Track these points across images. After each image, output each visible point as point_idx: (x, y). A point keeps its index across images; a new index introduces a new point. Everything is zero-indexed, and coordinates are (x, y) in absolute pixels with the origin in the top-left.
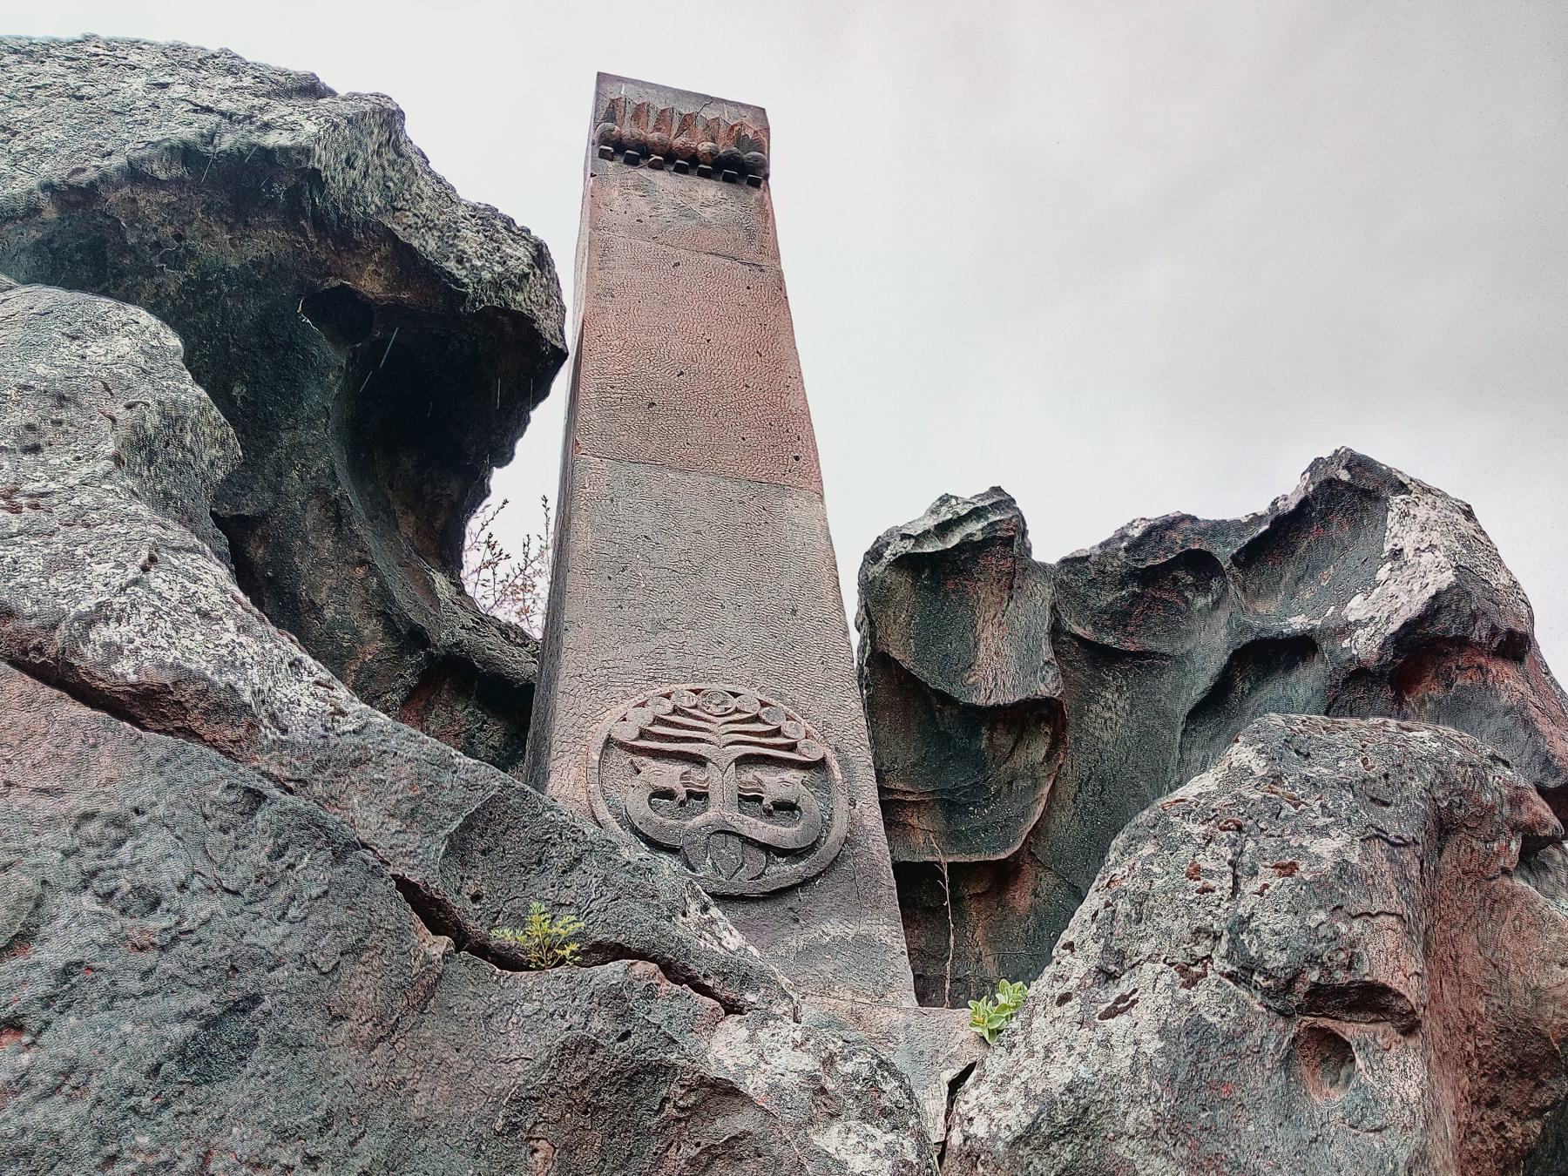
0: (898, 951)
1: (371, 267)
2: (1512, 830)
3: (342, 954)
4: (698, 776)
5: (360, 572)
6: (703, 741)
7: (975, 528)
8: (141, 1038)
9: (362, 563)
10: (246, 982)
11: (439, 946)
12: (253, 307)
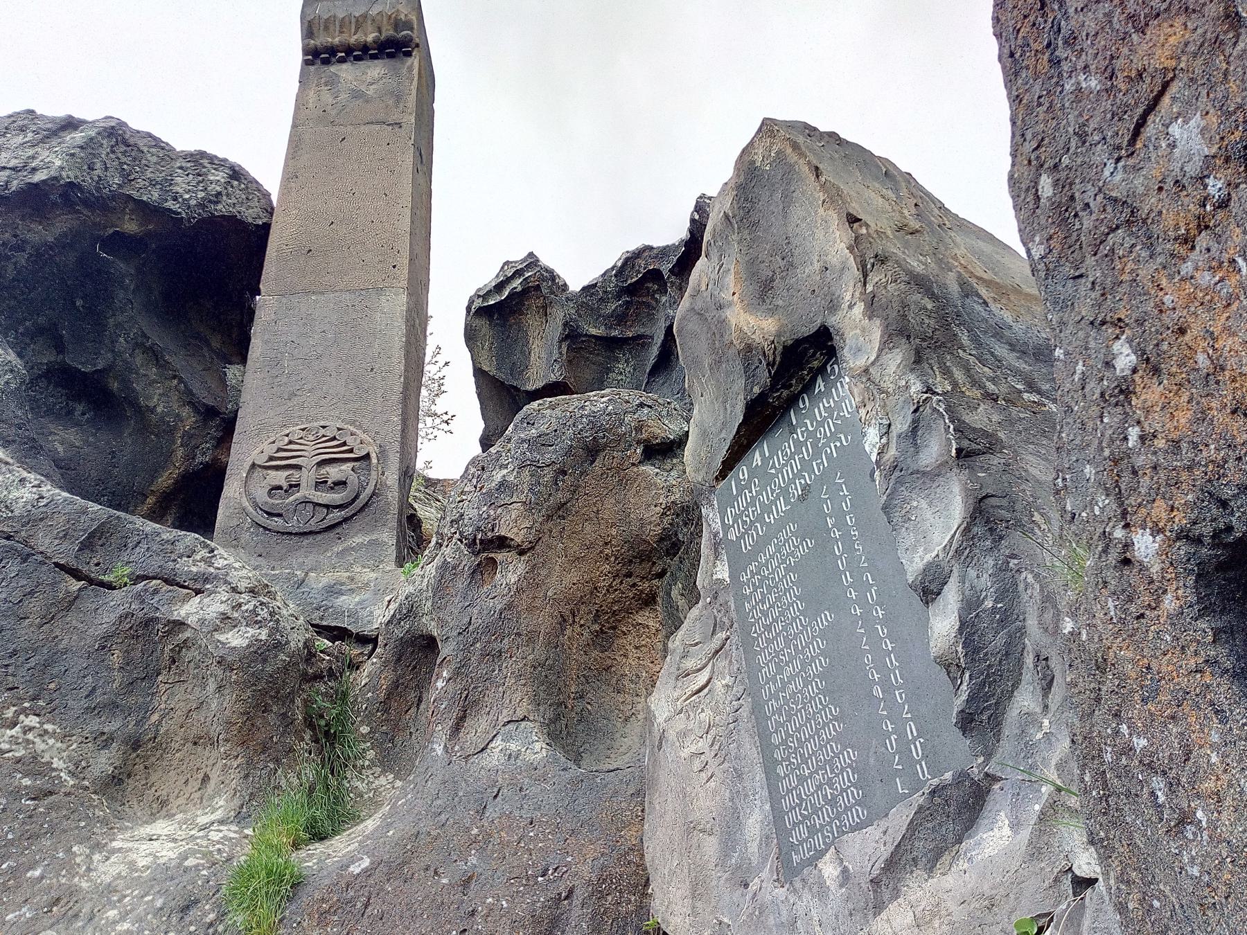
1: (127, 217)
2: (637, 443)
3: (24, 596)
4: (296, 474)
5: (175, 382)
6: (301, 456)
7: (517, 284)
9: (175, 377)
11: (75, 585)
12: (71, 258)
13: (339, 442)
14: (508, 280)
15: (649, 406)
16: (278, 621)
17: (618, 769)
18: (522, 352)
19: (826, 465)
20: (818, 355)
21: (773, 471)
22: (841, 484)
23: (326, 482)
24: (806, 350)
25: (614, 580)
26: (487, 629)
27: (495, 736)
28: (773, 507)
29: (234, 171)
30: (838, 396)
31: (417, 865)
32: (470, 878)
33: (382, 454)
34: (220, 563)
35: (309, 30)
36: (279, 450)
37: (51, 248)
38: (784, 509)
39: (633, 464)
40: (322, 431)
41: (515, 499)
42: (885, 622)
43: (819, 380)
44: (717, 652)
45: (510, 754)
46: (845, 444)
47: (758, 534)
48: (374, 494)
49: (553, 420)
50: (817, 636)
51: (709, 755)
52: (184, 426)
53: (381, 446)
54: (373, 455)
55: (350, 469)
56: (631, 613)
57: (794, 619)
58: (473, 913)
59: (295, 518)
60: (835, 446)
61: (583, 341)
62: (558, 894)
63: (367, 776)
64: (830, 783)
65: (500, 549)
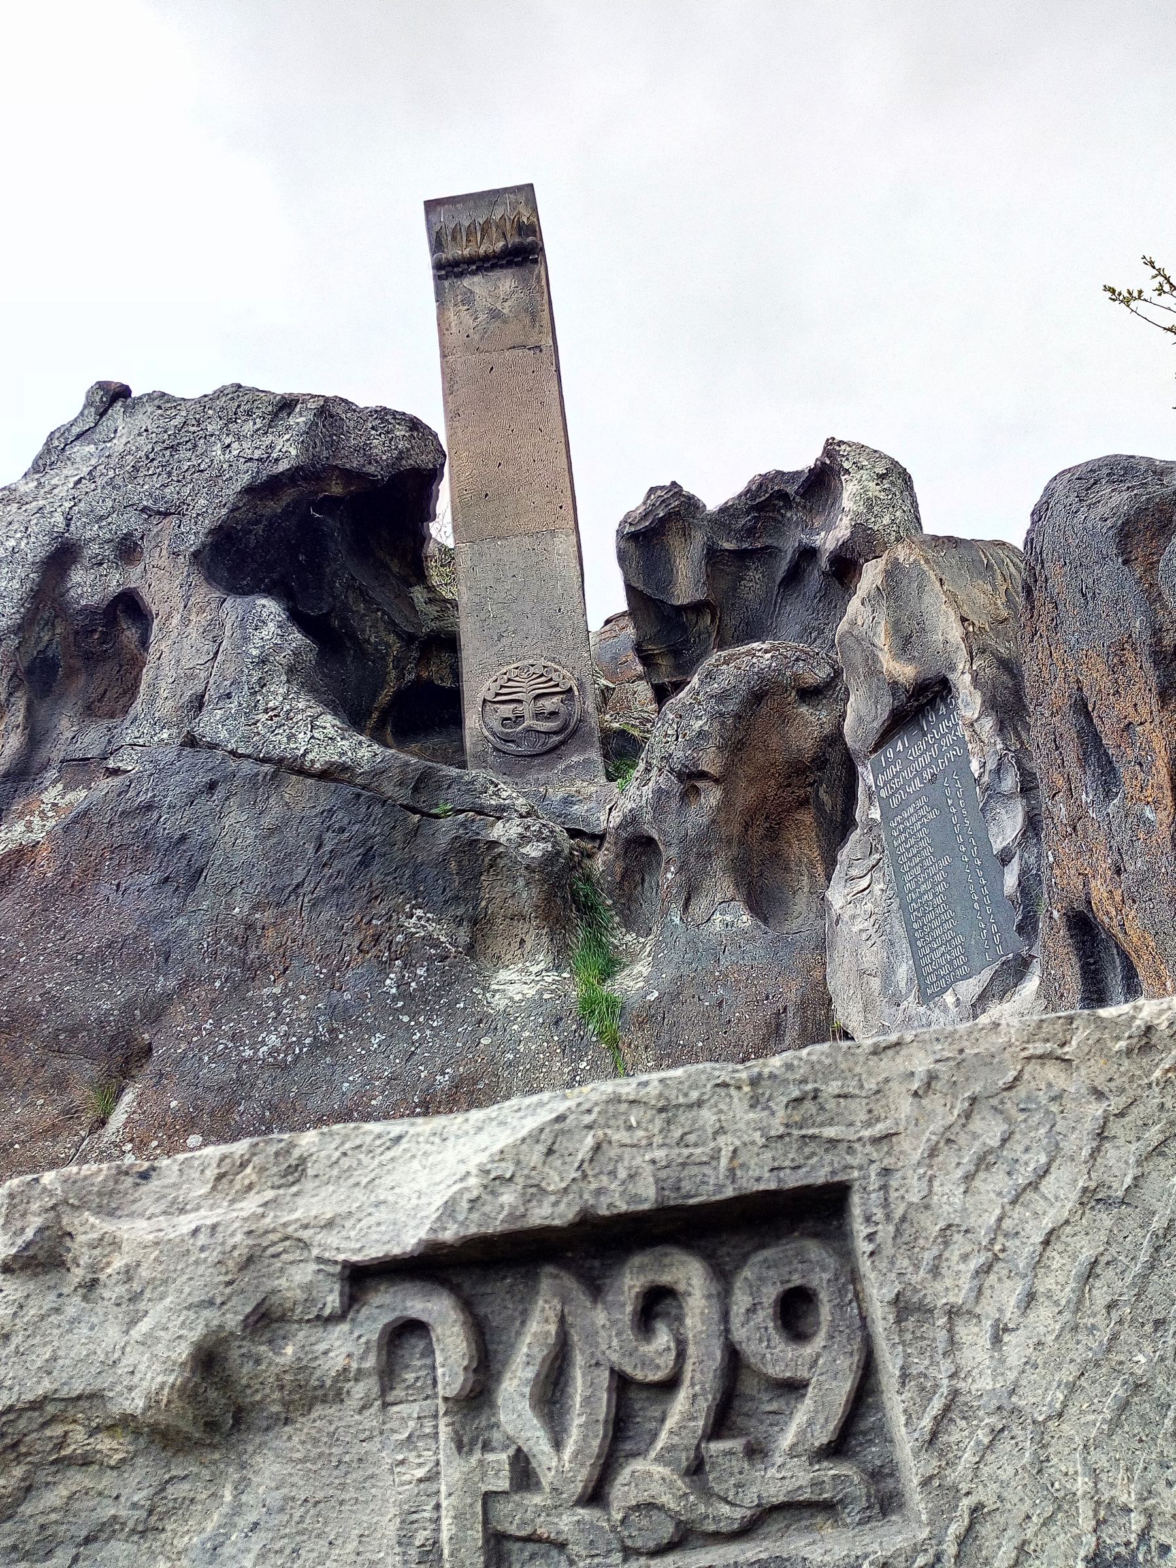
8: (351, 862)
9: (378, 610)
10: (369, 844)
11: (417, 817)
29: (414, 424)
33: (581, 686)
34: (504, 795)
35: (437, 244)
36: (502, 687)
37: (280, 518)
40: (532, 669)
51: (872, 931)
64: (949, 952)
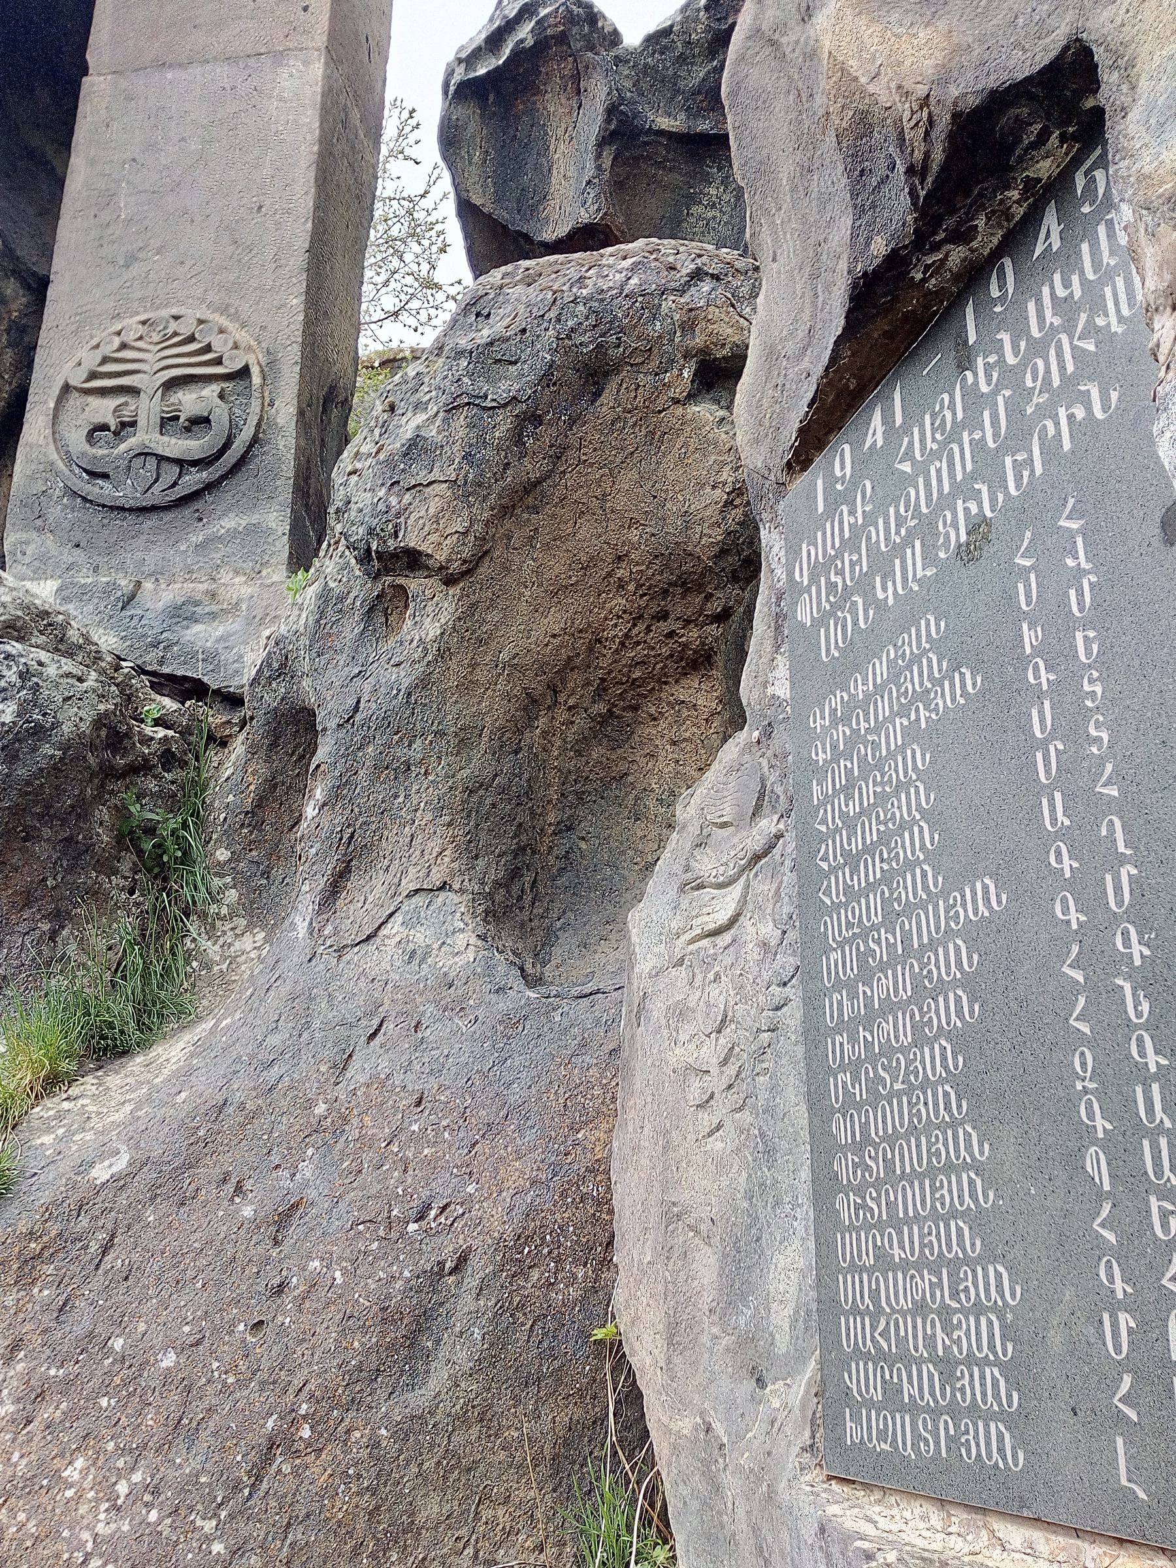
0: (280, 533)
2: (685, 357)
7: (525, 32)
13: (200, 345)
14: (509, 26)
15: (712, 276)
16: (36, 688)
17: (598, 992)
18: (537, 168)
19: (1039, 470)
20: (1054, 140)
21: (906, 467)
22: (1072, 534)
23: (177, 418)
24: (1021, 125)
25: (635, 625)
26: (385, 723)
27: (391, 915)
28: (897, 562)
30: (1097, 265)
31: (208, 1171)
32: (294, 1207)
36: (105, 360)
38: (920, 574)
39: (676, 401)
41: (436, 474)
42: (1146, 982)
43: (1051, 220)
44: (757, 858)
45: (414, 952)
46: (1099, 415)
47: (855, 623)
48: (255, 440)
49: (521, 309)
50: (958, 934)
51: (717, 1081)
52: (10, 312)
53: (269, 353)
54: (255, 371)
55: (215, 394)
56: (666, 683)
57: (910, 865)
58: (281, 1289)
59: (129, 481)
60: (1071, 417)
61: (646, 144)
62: (439, 1263)
63: (224, 933)
65: (412, 570)
